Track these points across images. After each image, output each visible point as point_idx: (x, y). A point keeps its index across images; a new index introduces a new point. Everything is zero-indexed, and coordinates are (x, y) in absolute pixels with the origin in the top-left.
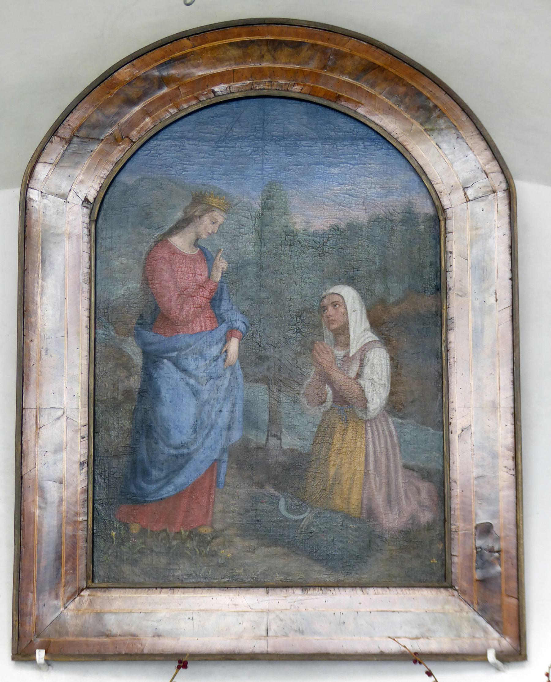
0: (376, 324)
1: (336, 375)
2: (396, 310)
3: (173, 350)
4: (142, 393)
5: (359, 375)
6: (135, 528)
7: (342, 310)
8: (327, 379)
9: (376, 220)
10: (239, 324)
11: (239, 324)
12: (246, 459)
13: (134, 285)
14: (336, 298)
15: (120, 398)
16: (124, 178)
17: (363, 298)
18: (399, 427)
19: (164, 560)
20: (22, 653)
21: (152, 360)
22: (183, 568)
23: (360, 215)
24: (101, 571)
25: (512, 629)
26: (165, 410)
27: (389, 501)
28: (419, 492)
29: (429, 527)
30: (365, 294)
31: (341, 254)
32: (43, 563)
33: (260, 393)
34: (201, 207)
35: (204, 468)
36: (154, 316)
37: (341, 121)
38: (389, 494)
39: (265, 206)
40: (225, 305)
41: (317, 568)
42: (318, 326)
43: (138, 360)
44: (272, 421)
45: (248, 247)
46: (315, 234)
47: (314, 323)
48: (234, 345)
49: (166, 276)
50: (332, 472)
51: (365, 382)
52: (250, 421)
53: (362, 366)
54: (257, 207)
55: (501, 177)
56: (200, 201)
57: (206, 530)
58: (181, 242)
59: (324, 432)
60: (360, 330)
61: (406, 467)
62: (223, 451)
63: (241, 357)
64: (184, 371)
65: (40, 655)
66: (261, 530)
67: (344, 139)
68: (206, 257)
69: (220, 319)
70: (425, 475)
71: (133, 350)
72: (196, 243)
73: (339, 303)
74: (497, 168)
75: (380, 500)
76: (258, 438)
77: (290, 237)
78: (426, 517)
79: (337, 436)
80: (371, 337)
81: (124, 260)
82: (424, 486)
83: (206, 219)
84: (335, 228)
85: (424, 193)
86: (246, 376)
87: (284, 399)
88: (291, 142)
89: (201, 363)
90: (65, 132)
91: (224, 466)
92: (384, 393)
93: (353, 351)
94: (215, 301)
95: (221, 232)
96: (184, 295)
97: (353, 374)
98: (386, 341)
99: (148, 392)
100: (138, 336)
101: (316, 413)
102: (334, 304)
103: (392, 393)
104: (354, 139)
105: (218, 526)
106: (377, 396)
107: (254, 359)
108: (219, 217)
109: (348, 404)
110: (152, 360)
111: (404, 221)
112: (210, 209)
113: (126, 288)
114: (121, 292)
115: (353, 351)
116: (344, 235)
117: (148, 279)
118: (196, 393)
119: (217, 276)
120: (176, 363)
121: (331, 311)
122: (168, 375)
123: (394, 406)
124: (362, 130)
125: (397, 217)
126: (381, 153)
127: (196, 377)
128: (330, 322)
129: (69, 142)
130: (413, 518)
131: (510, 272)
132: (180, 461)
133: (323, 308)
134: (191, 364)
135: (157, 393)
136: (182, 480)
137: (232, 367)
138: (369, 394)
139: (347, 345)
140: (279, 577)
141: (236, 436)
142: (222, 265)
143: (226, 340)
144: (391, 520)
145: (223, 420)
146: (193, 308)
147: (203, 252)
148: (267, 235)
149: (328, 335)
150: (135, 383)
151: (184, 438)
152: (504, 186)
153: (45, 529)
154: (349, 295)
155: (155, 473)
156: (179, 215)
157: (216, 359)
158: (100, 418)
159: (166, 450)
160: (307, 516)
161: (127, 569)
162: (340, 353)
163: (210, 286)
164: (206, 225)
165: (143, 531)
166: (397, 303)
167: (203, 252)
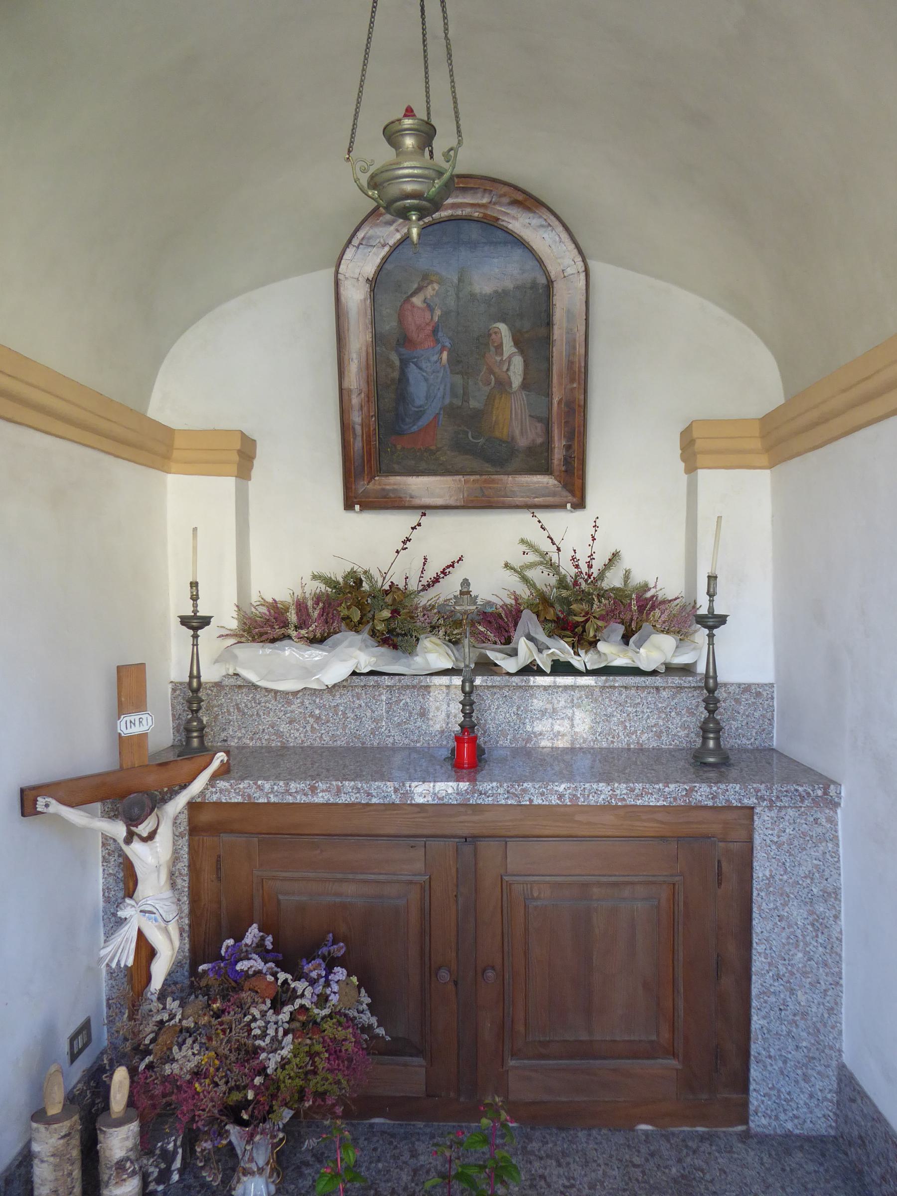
0: (517, 343)
1: (496, 370)
2: (526, 336)
3: (415, 357)
4: (400, 380)
5: (508, 370)
6: (399, 447)
7: (499, 335)
8: (491, 372)
9: (517, 288)
10: (448, 344)
11: (448, 344)
12: (452, 412)
13: (394, 324)
14: (496, 330)
15: (389, 382)
16: (387, 266)
17: (510, 329)
18: (527, 396)
19: (413, 462)
20: (349, 506)
21: (404, 363)
22: (423, 466)
23: (509, 284)
24: (384, 468)
25: (578, 493)
26: (412, 389)
27: (522, 433)
28: (536, 428)
29: (542, 445)
30: (512, 328)
31: (499, 306)
32: (356, 464)
33: (458, 380)
34: (426, 282)
35: (432, 417)
36: (405, 341)
37: (499, 233)
38: (522, 429)
39: (460, 280)
40: (440, 334)
41: (487, 465)
42: (487, 345)
43: (397, 363)
44: (464, 394)
45: (451, 302)
46: (485, 295)
47: (485, 342)
48: (445, 355)
49: (410, 319)
50: (494, 419)
51: (511, 373)
52: (454, 394)
53: (509, 365)
54: (456, 281)
55: (582, 264)
56: (426, 278)
57: (433, 448)
58: (417, 301)
59: (490, 398)
60: (508, 347)
61: (530, 416)
62: (441, 409)
63: (448, 360)
64: (420, 369)
65: (357, 507)
66: (460, 446)
67: (500, 243)
68: (430, 308)
69: (437, 341)
70: (540, 420)
71: (395, 358)
72: (425, 301)
73: (498, 332)
74: (580, 259)
75: (517, 432)
76: (458, 402)
77: (473, 295)
78: (539, 440)
79: (497, 401)
80: (514, 350)
81: (388, 310)
82: (539, 425)
83: (430, 287)
84: (496, 292)
85: (542, 273)
86: (451, 372)
87: (470, 383)
88: (473, 245)
89: (429, 364)
90: (355, 242)
91: (441, 417)
92: (520, 379)
93: (505, 357)
94: (435, 331)
95: (437, 294)
96: (419, 328)
97: (505, 369)
98: (522, 351)
99: (403, 379)
100: (397, 351)
101: (487, 389)
102: (496, 333)
103: (524, 379)
104: (505, 243)
105: (439, 446)
106: (516, 380)
107: (455, 361)
108: (436, 286)
109: (503, 385)
110: (404, 363)
111: (531, 288)
112: (432, 282)
113: (389, 325)
114: (387, 327)
115: (505, 357)
116: (501, 295)
117: (401, 320)
118: (426, 380)
119: (436, 319)
120: (416, 365)
121: (494, 336)
122: (413, 372)
123: (525, 386)
124: (510, 238)
125: (528, 285)
126: (518, 252)
127: (426, 372)
128: (494, 342)
129: (358, 247)
130: (533, 440)
131: (277, 644)
132: (419, 415)
133: (490, 335)
134: (424, 365)
135: (408, 380)
136: (423, 422)
137: (444, 366)
138: (513, 379)
139: (502, 354)
140: (468, 470)
141: (447, 401)
142: (438, 312)
143: (441, 353)
144: (523, 442)
145: (440, 394)
146: (814, 1023)
147: (429, 306)
148: (461, 295)
149: (493, 349)
150: (396, 375)
151: (422, 403)
152: (583, 269)
153: (356, 449)
154: (503, 327)
155: (407, 420)
156: (415, 286)
157: (436, 362)
158: (380, 393)
159: (414, 409)
160: (481, 441)
161: (396, 467)
162: (498, 359)
163: (432, 324)
164: (430, 291)
165: (403, 448)
166: (527, 332)
167: (429, 306)
